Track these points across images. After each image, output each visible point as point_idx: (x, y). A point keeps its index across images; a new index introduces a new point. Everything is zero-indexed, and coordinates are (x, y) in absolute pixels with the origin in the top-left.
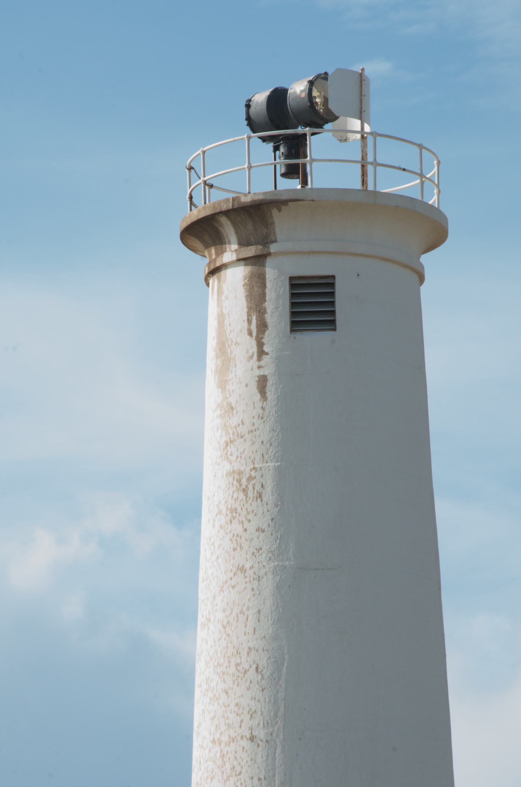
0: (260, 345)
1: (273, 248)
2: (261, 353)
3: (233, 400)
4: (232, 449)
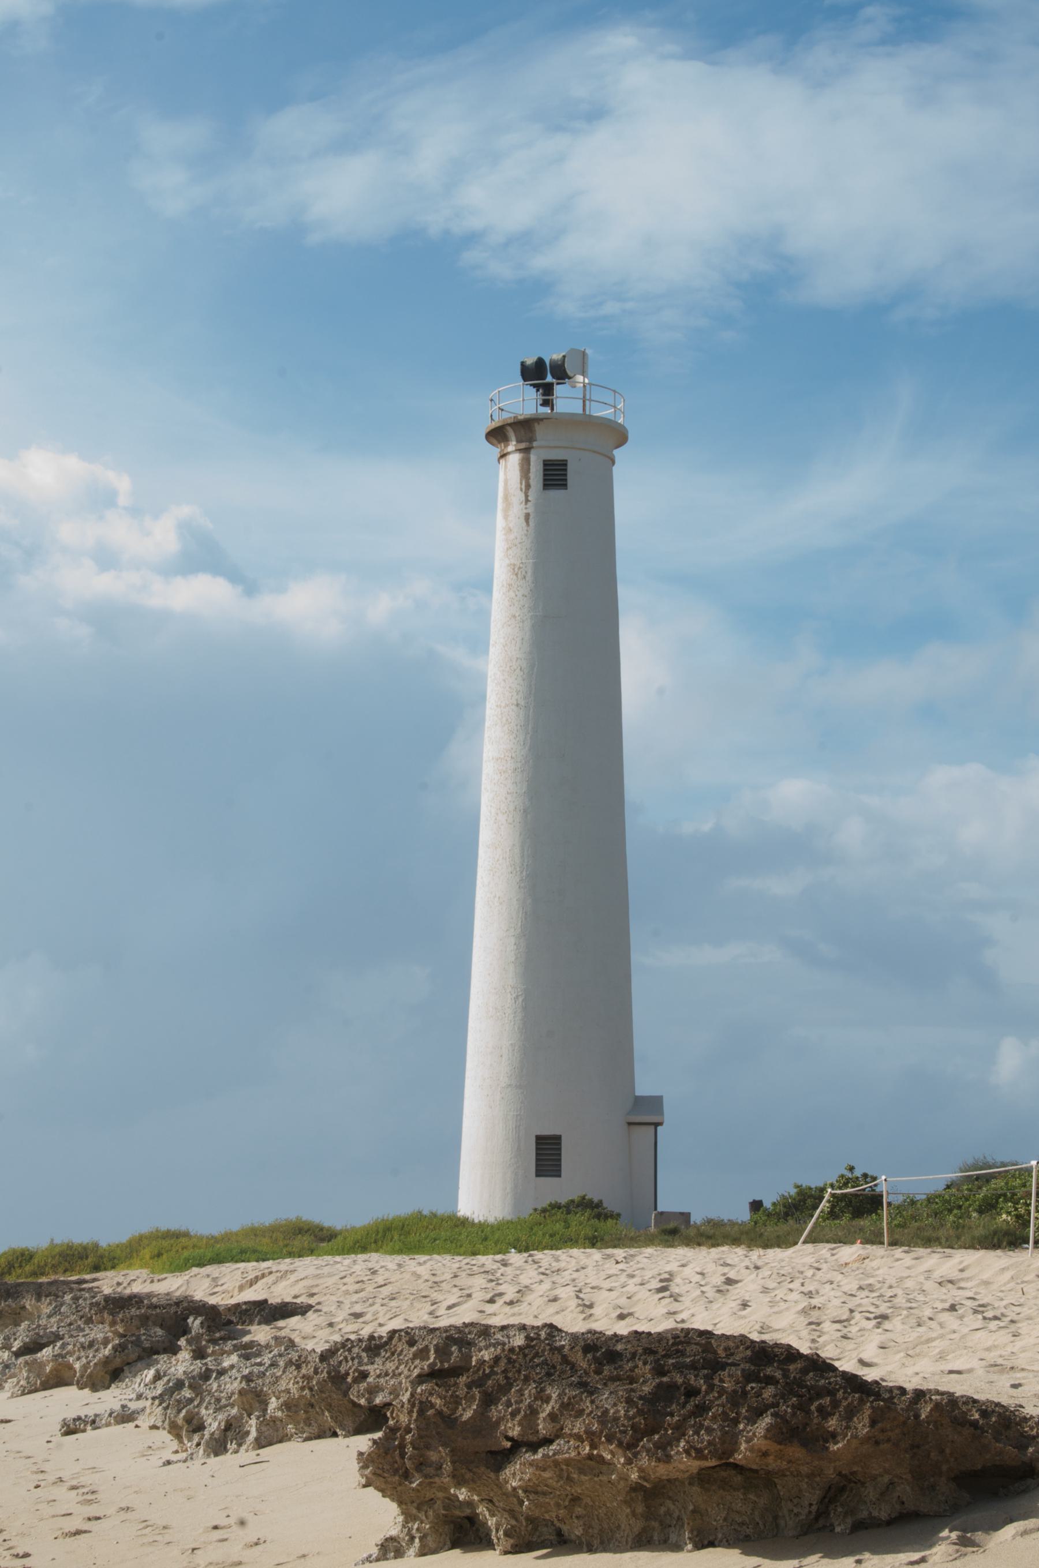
0: (527, 496)
1: (535, 444)
2: (527, 501)
3: (511, 525)
4: (510, 552)
